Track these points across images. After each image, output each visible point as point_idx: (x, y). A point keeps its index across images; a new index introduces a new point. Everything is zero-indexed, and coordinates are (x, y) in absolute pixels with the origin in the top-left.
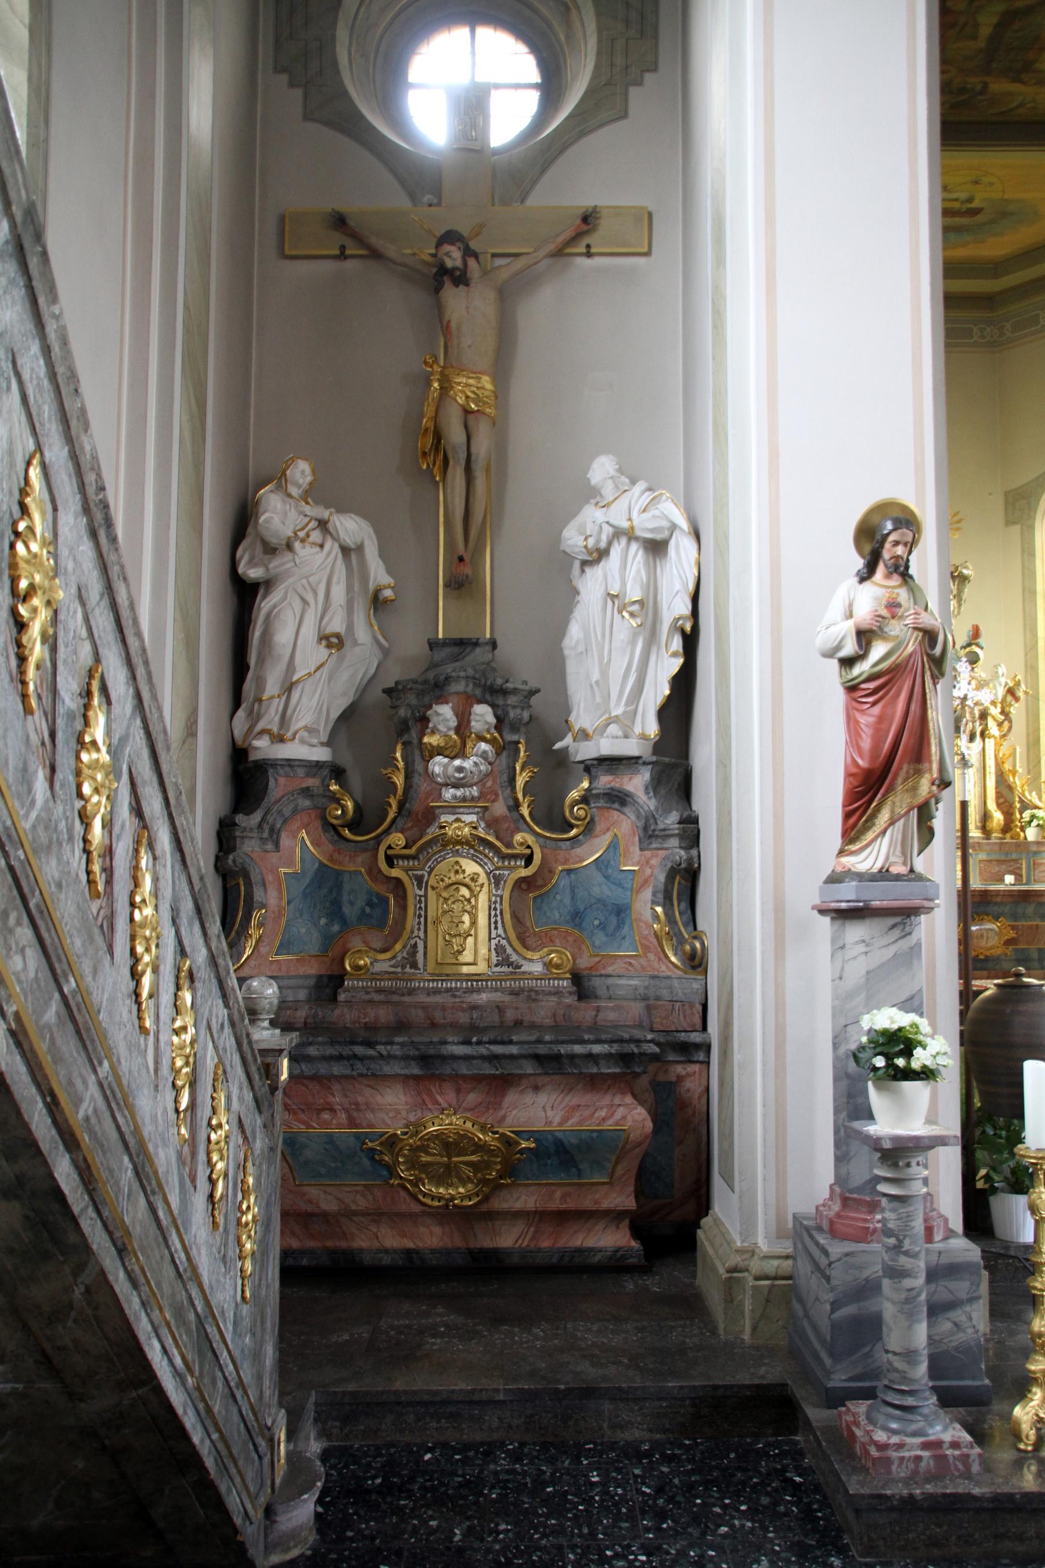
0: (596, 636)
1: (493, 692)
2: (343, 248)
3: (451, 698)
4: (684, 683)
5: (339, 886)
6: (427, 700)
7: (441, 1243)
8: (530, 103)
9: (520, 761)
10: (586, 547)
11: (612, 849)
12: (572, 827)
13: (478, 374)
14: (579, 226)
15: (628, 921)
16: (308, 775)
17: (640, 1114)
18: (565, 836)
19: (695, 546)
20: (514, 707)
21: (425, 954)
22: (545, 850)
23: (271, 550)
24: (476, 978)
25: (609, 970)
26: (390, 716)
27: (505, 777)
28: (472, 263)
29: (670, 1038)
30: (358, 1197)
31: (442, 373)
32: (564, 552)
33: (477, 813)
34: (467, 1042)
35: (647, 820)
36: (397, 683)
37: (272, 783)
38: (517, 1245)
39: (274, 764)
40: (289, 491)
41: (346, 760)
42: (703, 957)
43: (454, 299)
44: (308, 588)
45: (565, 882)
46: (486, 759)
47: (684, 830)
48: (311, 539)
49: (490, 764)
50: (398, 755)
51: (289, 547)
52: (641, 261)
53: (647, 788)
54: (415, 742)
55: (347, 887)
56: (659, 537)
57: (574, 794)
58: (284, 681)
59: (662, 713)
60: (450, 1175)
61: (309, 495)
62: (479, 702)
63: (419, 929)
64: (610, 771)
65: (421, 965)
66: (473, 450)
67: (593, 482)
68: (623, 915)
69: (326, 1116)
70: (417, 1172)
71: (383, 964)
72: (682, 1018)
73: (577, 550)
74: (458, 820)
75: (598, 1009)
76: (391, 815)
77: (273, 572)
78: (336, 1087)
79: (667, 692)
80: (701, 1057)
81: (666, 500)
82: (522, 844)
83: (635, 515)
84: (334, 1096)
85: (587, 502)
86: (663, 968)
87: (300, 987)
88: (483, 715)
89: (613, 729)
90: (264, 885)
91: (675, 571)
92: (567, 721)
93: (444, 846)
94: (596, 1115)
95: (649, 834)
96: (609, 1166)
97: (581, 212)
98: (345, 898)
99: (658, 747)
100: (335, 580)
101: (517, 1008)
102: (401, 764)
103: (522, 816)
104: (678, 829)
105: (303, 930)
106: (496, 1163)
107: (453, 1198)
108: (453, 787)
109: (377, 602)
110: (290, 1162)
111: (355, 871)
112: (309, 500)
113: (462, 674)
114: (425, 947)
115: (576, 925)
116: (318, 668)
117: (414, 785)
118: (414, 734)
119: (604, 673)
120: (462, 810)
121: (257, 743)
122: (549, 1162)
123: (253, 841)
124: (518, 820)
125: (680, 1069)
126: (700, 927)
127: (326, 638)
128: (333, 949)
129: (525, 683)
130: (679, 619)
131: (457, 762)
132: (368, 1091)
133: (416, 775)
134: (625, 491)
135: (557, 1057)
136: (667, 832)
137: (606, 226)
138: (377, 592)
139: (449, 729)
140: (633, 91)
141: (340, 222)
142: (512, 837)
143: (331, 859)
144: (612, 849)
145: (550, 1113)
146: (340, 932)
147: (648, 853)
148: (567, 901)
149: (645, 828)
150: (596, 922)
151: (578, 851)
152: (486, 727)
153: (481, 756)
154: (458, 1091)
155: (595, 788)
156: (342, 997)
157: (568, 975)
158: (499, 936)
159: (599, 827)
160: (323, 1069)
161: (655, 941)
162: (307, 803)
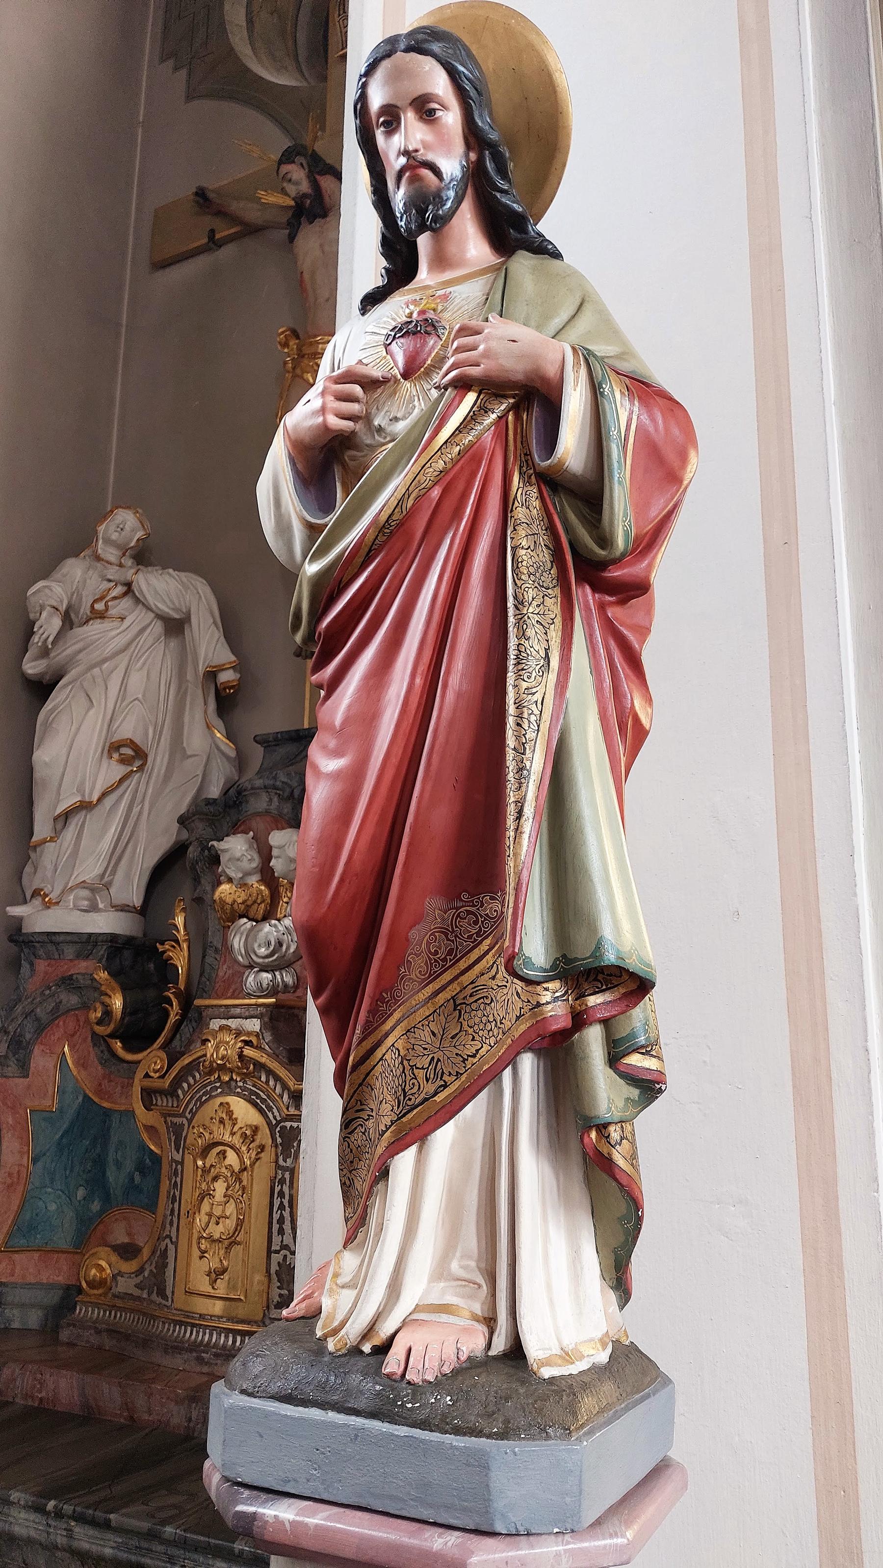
5: (103, 1137)
16: (79, 956)
33: (260, 1017)
55: (114, 1139)
65: (169, 1293)
76: (173, 1018)
87: (33, 1306)
105: (53, 1207)
143: (99, 1092)
146: (102, 1211)
156: (65, 1335)
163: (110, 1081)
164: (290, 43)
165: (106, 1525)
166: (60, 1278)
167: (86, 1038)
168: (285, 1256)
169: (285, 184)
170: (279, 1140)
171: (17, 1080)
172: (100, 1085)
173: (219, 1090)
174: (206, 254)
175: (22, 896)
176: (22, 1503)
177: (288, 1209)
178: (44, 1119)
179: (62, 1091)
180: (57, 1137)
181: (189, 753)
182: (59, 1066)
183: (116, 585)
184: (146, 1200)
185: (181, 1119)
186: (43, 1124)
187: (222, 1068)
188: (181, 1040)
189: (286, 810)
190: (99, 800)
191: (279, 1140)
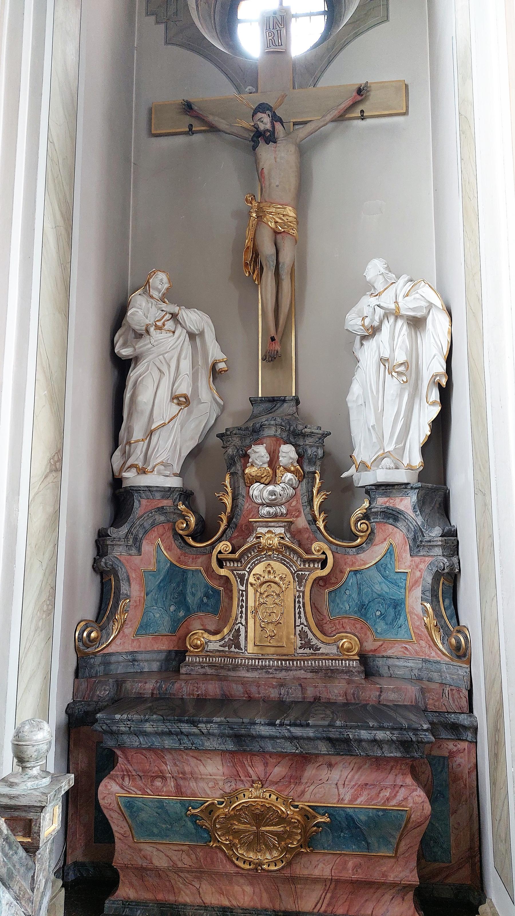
0: (372, 392)
1: (294, 436)
3: (265, 441)
4: (442, 425)
5: (184, 581)
6: (248, 441)
7: (252, 904)
8: (320, 24)
9: (316, 486)
10: (363, 325)
11: (388, 555)
12: (357, 537)
13: (284, 205)
16: (163, 498)
17: (420, 796)
19: (448, 319)
20: (311, 446)
21: (246, 637)
22: (337, 555)
23: (139, 336)
24: (286, 658)
25: (389, 653)
26: (222, 453)
27: (305, 499)
28: (278, 126)
29: (442, 719)
30: (184, 855)
31: (258, 206)
34: (272, 724)
35: (415, 533)
36: (227, 430)
37: (136, 504)
38: (316, 910)
39: (137, 490)
40: (151, 294)
41: (194, 485)
42: (467, 649)
43: (266, 153)
44: (163, 361)
45: (352, 580)
46: (291, 485)
47: (446, 542)
50: (227, 482)
51: (148, 332)
53: (414, 508)
54: (240, 472)
55: (190, 582)
56: (418, 314)
58: (147, 430)
59: (425, 449)
60: (259, 843)
61: (167, 296)
63: (241, 617)
64: (385, 494)
65: (243, 646)
66: (281, 260)
67: (368, 278)
69: (158, 783)
70: (231, 838)
71: (214, 643)
72: (451, 701)
73: (356, 328)
74: (269, 532)
75: (381, 690)
77: (138, 351)
78: (168, 757)
80: (470, 736)
82: (319, 551)
83: (400, 299)
84: (166, 764)
85: (365, 294)
86: (433, 654)
87: (154, 661)
88: (288, 453)
89: (387, 462)
91: (432, 340)
92: (351, 457)
93: (260, 551)
94: (381, 795)
95: (417, 544)
96: (394, 841)
97: (356, 87)
99: (422, 476)
100: (183, 356)
101: (316, 687)
102: (229, 490)
104: (442, 541)
105: (157, 615)
106: (297, 834)
107: (260, 864)
108: (268, 506)
109: (215, 373)
110: (130, 821)
111: (197, 570)
112: (166, 300)
113: (273, 422)
114: (246, 632)
115: (362, 615)
116: (171, 420)
117: (240, 505)
118: (239, 467)
119: (379, 416)
120: (273, 524)
121: (125, 475)
122: (342, 835)
123: (121, 549)
125: (451, 746)
126: (462, 623)
127: (177, 397)
128: (179, 629)
130: (436, 375)
131: (271, 488)
132: (193, 762)
133: (240, 497)
135: (347, 741)
136: (432, 543)
137: (375, 97)
138: (214, 365)
139: (264, 463)
141: (188, 108)
144: (388, 555)
145: (341, 790)
146: (185, 617)
147: (417, 559)
148: (355, 596)
149: (415, 539)
150: (378, 613)
151: (362, 556)
152: (291, 461)
153: (288, 483)
154: (266, 764)
155: (374, 508)
156: (183, 670)
157: (357, 657)
158: (303, 624)
159: (378, 537)
160: (157, 742)
161: (425, 631)
162: (162, 518)
165: (308, 725)
166: (164, 647)
168: (302, 628)
169: (258, 123)
170: (297, 579)
172: (179, 558)
173: (265, 559)
176: (262, 723)
178: (150, 575)
179: (158, 562)
180: (157, 583)
185: (243, 572)
187: (270, 549)
190: (169, 423)
191: (297, 579)
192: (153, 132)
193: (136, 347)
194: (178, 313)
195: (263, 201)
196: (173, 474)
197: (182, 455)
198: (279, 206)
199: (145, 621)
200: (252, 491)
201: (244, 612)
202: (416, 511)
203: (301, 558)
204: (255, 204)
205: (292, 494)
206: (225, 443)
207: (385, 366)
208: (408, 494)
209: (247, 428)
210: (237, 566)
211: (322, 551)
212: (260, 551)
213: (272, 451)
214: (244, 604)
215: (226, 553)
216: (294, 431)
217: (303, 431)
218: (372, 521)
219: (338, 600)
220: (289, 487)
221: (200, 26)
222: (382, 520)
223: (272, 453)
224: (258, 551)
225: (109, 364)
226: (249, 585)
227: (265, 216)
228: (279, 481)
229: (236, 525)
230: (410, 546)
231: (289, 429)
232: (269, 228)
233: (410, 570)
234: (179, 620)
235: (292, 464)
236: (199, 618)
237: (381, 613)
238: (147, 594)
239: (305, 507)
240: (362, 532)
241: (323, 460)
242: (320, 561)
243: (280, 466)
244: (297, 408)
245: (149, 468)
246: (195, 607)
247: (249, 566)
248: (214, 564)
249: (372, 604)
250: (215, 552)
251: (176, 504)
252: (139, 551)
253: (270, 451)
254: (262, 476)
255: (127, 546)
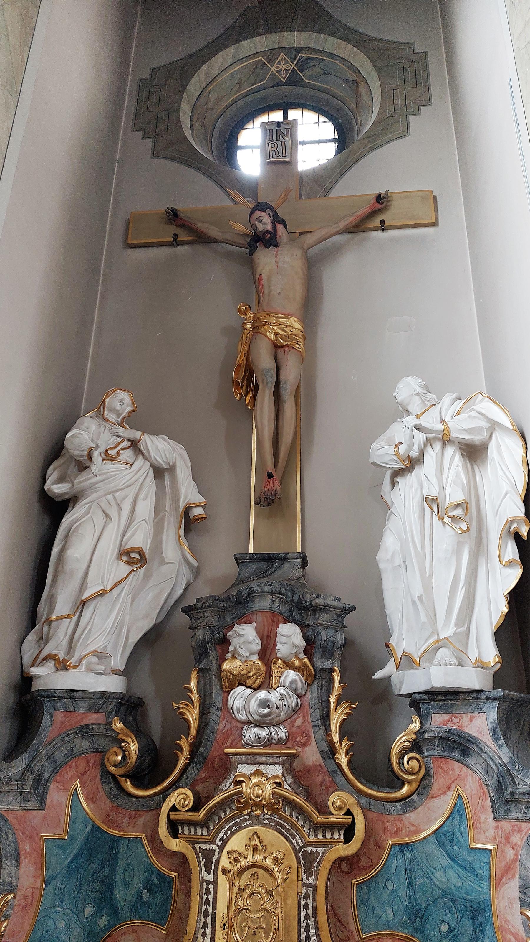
1: (301, 609)
2: (175, 236)
3: (254, 617)
6: (228, 619)
9: (335, 693)
10: (397, 454)
11: (455, 816)
14: (374, 204)
15: (489, 931)
16: (91, 709)
18: (393, 795)
19: (521, 443)
20: (326, 627)
22: (370, 815)
26: (188, 639)
27: (317, 714)
28: (280, 228)
32: (374, 464)
36: (198, 600)
37: (46, 719)
39: (51, 696)
41: (146, 689)
43: (266, 260)
44: (113, 503)
45: (397, 863)
46: (295, 691)
48: (121, 457)
49: (299, 696)
52: (430, 230)
53: (494, 733)
54: (214, 669)
55: (122, 862)
56: (477, 438)
57: (402, 740)
59: (500, 635)
62: (286, 621)
64: (444, 709)
66: (282, 377)
67: (400, 399)
68: (480, 919)
73: (387, 459)
74: (258, 773)
77: (77, 487)
79: (506, 610)
81: (482, 401)
82: (340, 808)
88: (290, 637)
89: (443, 654)
90: (17, 857)
92: (387, 645)
93: (241, 809)
98: (119, 876)
99: (498, 679)
100: (142, 496)
102: (195, 697)
103: (339, 766)
105: (61, 924)
108: (256, 726)
109: (189, 523)
115: (416, 930)
116: (116, 586)
117: (211, 723)
118: (212, 659)
119: (428, 582)
120: (263, 758)
121: (35, 671)
123: (10, 798)
124: (333, 772)
127: (127, 553)
129: (338, 599)
130: (512, 522)
131: (262, 694)
133: (213, 710)
134: (433, 405)
139: (252, 654)
140: (411, 118)
141: (173, 216)
142: (328, 795)
143: (107, 821)
144: (455, 816)
146: (109, 927)
147: (506, 826)
148: (402, 891)
149: (500, 789)
150: (444, 928)
151: (412, 817)
152: (294, 650)
153: (290, 688)
155: (428, 731)
159: (436, 785)
162: (86, 745)
163: (118, 813)
164: (209, 146)
167: (95, 777)
169: (257, 222)
170: (302, 862)
171: (35, 813)
172: (108, 816)
174: (166, 247)
175: (19, 659)
177: (312, 919)
178: (57, 846)
179: (72, 821)
180: (68, 861)
181: (167, 561)
182: (72, 801)
183: (124, 440)
184: (154, 914)
185: (211, 846)
186: (56, 851)
187: (257, 805)
188: (187, 779)
189: (284, 610)
190: (111, 590)
191: (302, 862)
192: (129, 242)
193: (76, 481)
194: (140, 440)
195: (261, 311)
196: (112, 671)
197: (130, 641)
198: (281, 316)
199: (39, 934)
200: (232, 700)
201: (209, 926)
202: (499, 739)
203: (310, 821)
204: (250, 315)
205: (296, 706)
206: (193, 621)
207: (432, 509)
208: (481, 709)
209: (229, 597)
210: (202, 835)
211: (346, 809)
212: (242, 807)
213: (266, 633)
214: (210, 909)
215: (184, 810)
216: (300, 601)
217: (314, 603)
218: (426, 754)
219: (373, 901)
220: (291, 693)
221: (193, 142)
222: (442, 753)
223: (265, 637)
224: (238, 808)
225: (36, 507)
226: (220, 873)
227: (262, 326)
228: (275, 683)
229: (204, 759)
230: (492, 801)
231: (292, 600)
232: (267, 339)
233: (495, 847)
234: (97, 933)
235: (296, 655)
236: (134, 931)
237: (450, 928)
238: (47, 883)
239: (317, 729)
240: (411, 774)
241: (344, 649)
242: (342, 827)
243: (278, 659)
244: (303, 571)
245: (73, 661)
246: (127, 908)
247: (221, 835)
248: (163, 830)
249: (432, 908)
250: (166, 807)
251: (110, 720)
252: (41, 803)
253: (263, 635)
254: (250, 675)
255: (21, 793)
